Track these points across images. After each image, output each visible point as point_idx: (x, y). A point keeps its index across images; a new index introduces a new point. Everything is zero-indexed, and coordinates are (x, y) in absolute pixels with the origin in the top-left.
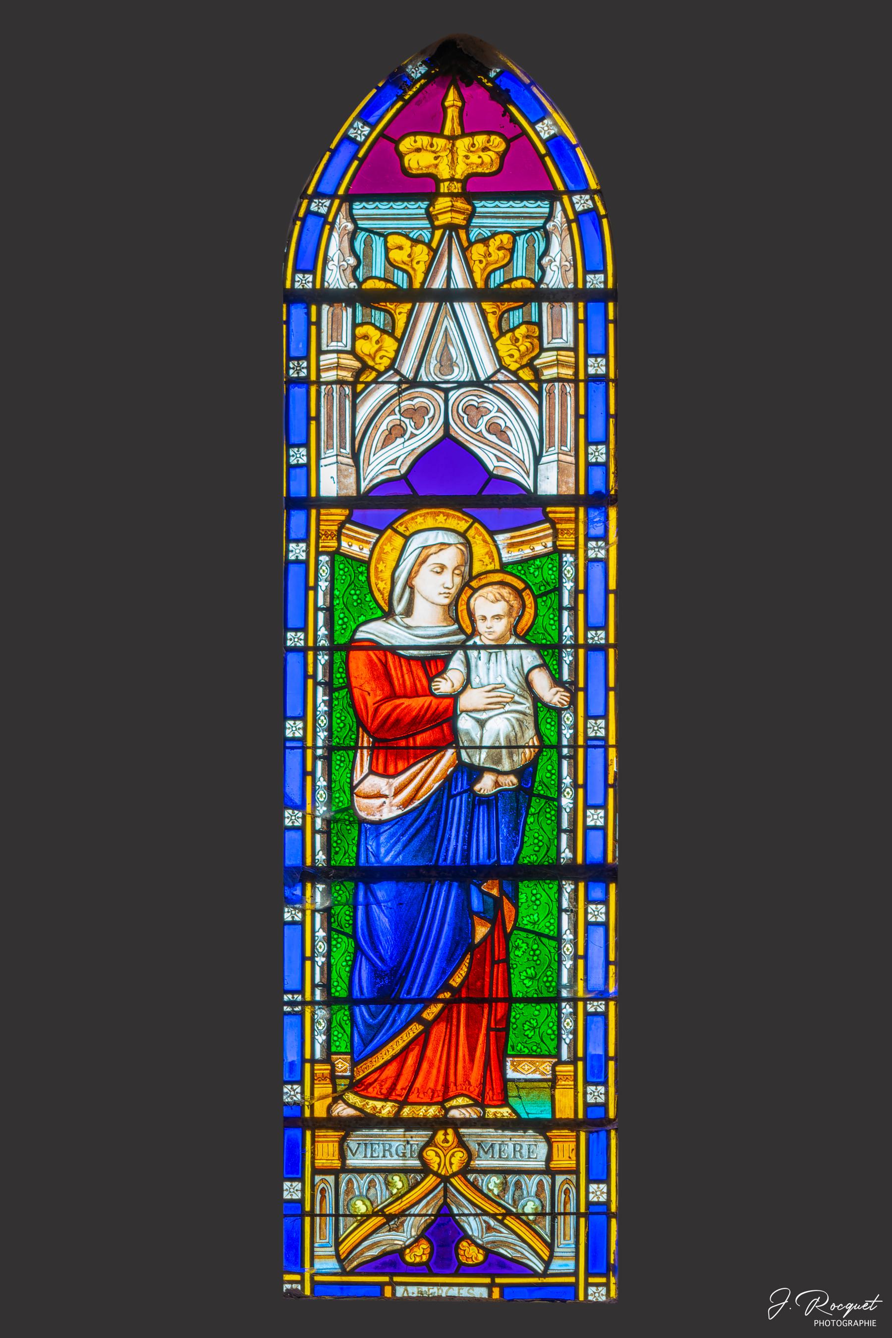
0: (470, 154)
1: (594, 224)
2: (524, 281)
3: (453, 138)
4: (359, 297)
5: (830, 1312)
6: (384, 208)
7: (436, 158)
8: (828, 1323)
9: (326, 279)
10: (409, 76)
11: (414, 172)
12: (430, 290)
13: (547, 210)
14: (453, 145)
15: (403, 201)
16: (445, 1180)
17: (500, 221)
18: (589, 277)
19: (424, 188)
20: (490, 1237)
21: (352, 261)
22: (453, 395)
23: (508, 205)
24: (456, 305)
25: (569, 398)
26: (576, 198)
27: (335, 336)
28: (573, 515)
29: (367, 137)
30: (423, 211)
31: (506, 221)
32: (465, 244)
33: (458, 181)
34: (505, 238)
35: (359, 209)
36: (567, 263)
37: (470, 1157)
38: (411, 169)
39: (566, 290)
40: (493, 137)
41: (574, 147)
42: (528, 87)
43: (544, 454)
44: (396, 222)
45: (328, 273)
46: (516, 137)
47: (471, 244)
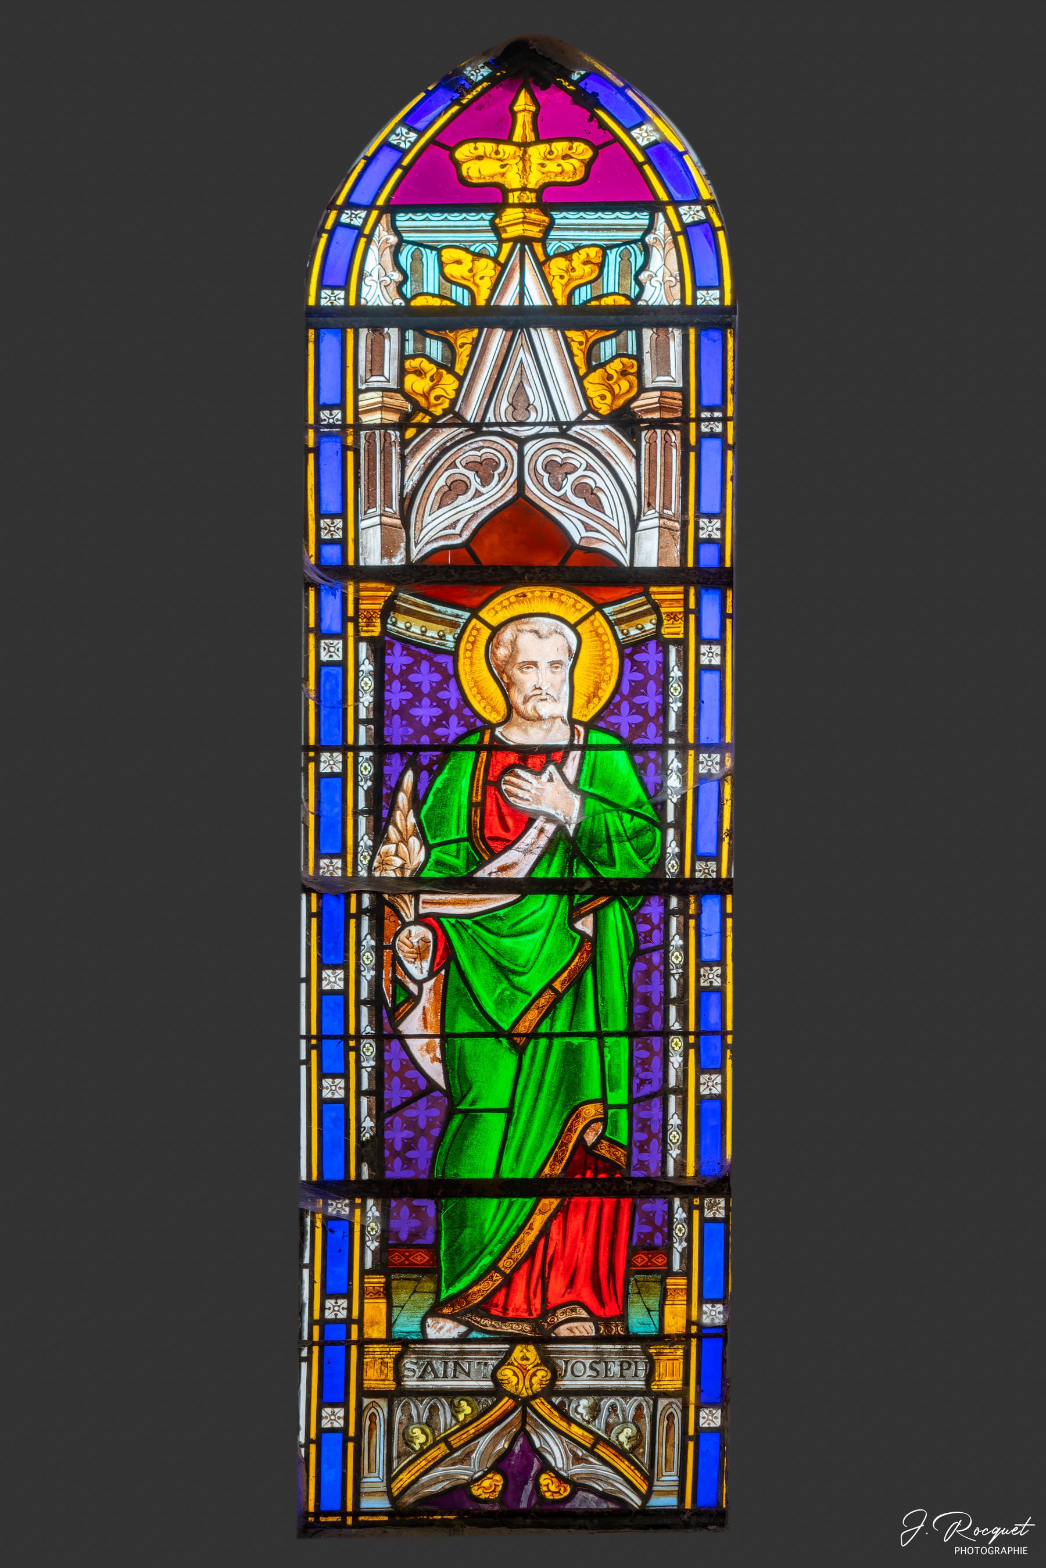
0: (546, 162)
1: (706, 236)
2: (617, 297)
3: (524, 145)
4: (410, 318)
5: (974, 1537)
6: (436, 219)
7: (503, 166)
8: (970, 1551)
9: (363, 295)
10: (467, 79)
11: (475, 181)
12: (498, 309)
13: (647, 222)
14: (525, 152)
15: (461, 212)
16: (524, 1403)
17: (586, 233)
18: (700, 294)
19: (491, 198)
20: (577, 1470)
21: (397, 276)
22: (530, 448)
23: (596, 216)
24: (532, 330)
25: (674, 451)
26: (683, 209)
27: (376, 366)
28: (681, 596)
29: (413, 144)
30: (487, 223)
31: (594, 233)
32: (542, 258)
33: (531, 191)
34: (593, 252)
35: (403, 220)
36: (672, 279)
37: (555, 1375)
38: (470, 178)
39: (670, 308)
40: (576, 144)
41: (680, 155)
42: (621, 91)
43: (643, 518)
44: (451, 235)
45: (365, 290)
46: (607, 144)
47: (549, 258)
